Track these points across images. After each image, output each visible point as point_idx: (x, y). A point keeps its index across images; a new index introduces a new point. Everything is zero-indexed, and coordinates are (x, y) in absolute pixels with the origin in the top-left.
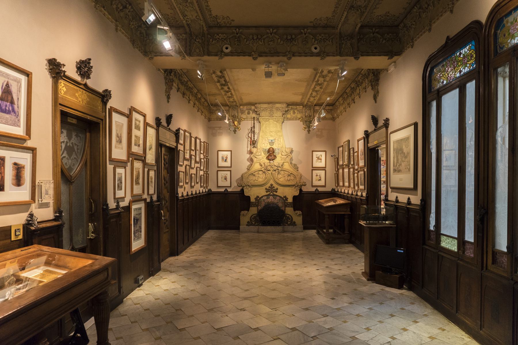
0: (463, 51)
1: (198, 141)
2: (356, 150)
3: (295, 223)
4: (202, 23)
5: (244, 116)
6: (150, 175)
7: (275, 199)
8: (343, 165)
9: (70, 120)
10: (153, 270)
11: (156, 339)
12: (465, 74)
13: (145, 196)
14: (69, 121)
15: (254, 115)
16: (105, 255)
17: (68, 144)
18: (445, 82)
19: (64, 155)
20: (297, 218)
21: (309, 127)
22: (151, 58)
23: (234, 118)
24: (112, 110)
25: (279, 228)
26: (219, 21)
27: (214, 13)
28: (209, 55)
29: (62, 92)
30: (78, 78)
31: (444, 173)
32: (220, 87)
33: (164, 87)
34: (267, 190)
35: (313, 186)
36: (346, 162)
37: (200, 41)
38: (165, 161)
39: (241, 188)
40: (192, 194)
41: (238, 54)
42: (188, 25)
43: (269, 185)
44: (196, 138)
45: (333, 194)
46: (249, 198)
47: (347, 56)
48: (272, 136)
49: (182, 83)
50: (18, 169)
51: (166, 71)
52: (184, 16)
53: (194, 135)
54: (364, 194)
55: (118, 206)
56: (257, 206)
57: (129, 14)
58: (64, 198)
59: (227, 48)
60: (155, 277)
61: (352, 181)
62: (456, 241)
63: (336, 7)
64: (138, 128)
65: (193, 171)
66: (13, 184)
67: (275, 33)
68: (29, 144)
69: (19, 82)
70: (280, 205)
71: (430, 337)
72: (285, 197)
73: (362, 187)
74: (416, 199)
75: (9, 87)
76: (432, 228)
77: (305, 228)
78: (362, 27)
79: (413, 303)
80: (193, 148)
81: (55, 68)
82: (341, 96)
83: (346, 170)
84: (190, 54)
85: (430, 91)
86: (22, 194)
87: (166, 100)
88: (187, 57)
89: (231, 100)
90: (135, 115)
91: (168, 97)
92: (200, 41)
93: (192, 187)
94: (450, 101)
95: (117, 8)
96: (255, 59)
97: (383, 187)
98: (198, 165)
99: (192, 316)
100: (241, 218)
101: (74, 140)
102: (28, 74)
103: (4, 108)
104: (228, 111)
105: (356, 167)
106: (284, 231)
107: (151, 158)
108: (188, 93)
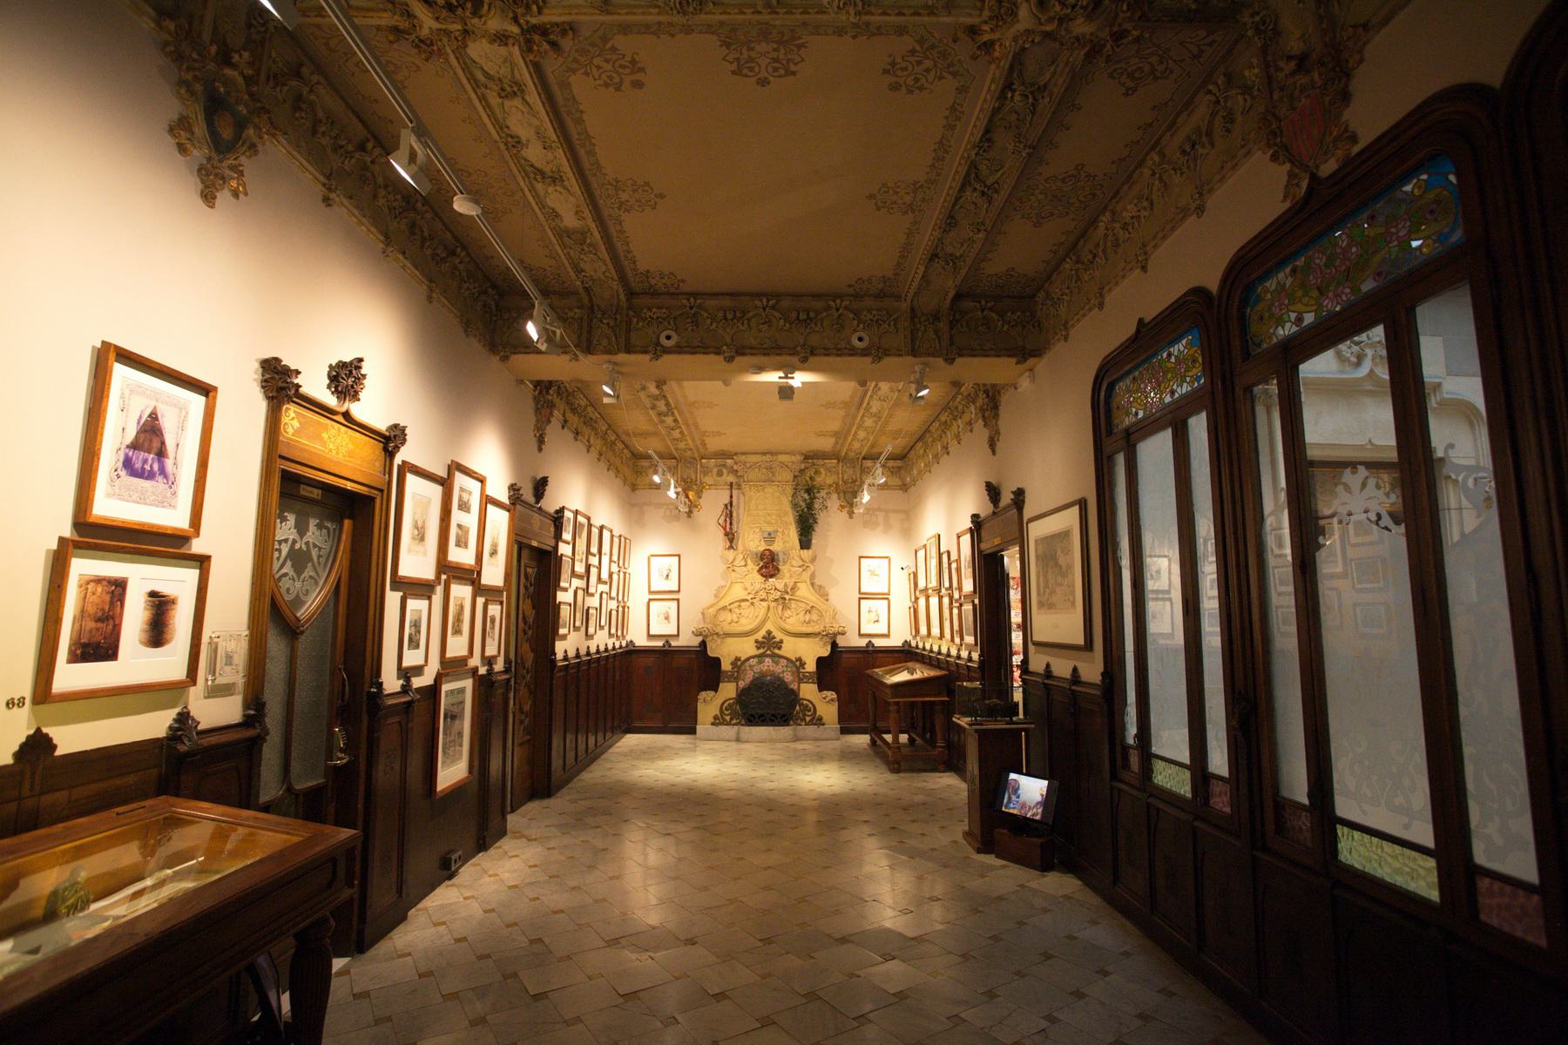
0: (1175, 350)
1: (606, 534)
2: (954, 556)
3: (820, 719)
4: (615, 285)
5: (708, 480)
6: (490, 613)
7: (777, 663)
8: (926, 589)
9: (305, 491)
10: (485, 837)
11: (473, 1023)
12: (1183, 397)
13: (475, 661)
14: (303, 493)
15: (731, 478)
16: (341, 822)
17: (297, 546)
18: (1141, 414)
19: (284, 571)
20: (826, 705)
21: (851, 505)
22: (505, 359)
23: (687, 485)
24: (406, 468)
25: (785, 731)
26: (653, 282)
27: (642, 267)
28: (629, 352)
29: (290, 430)
30: (331, 400)
31: (1152, 607)
32: (655, 419)
33: (532, 419)
34: (759, 644)
35: (860, 635)
36: (934, 583)
37: (612, 323)
38: (527, 578)
39: (700, 639)
40: (588, 654)
41: (693, 350)
42: (587, 289)
43: (763, 632)
44: (601, 528)
45: (906, 654)
46: (717, 661)
47: (928, 355)
48: (769, 523)
49: (574, 411)
50: (160, 606)
51: (537, 384)
52: (579, 271)
53: (597, 522)
54: (975, 656)
55: (406, 689)
56: (736, 680)
57: (461, 267)
58: (276, 669)
59: (668, 338)
60: (492, 851)
61: (947, 624)
62: (1188, 774)
63: (902, 257)
64: (464, 507)
65: (593, 602)
66: (141, 643)
67: (773, 307)
68: (197, 546)
69: (183, 409)
70: (788, 677)
71: (1140, 1016)
72: (799, 659)
73: (969, 639)
74: (1092, 671)
75: (156, 419)
76: (1131, 741)
77: (844, 731)
78: (958, 297)
79: (1094, 922)
80: (594, 549)
81: (278, 382)
82: (920, 439)
83: (934, 601)
84: (589, 350)
85: (1110, 433)
86: (168, 664)
87: (534, 442)
88: (581, 356)
89: (682, 445)
90: (460, 480)
91: (541, 441)
92: (612, 323)
93: (588, 636)
94: (1156, 452)
95: (434, 255)
96: (730, 360)
97: (1017, 638)
98: (605, 588)
99: (569, 957)
100: (700, 706)
101: (313, 534)
102: (206, 390)
103: (138, 465)
104: (673, 470)
105: (956, 596)
106: (796, 739)
107: (494, 574)
108: (586, 430)
